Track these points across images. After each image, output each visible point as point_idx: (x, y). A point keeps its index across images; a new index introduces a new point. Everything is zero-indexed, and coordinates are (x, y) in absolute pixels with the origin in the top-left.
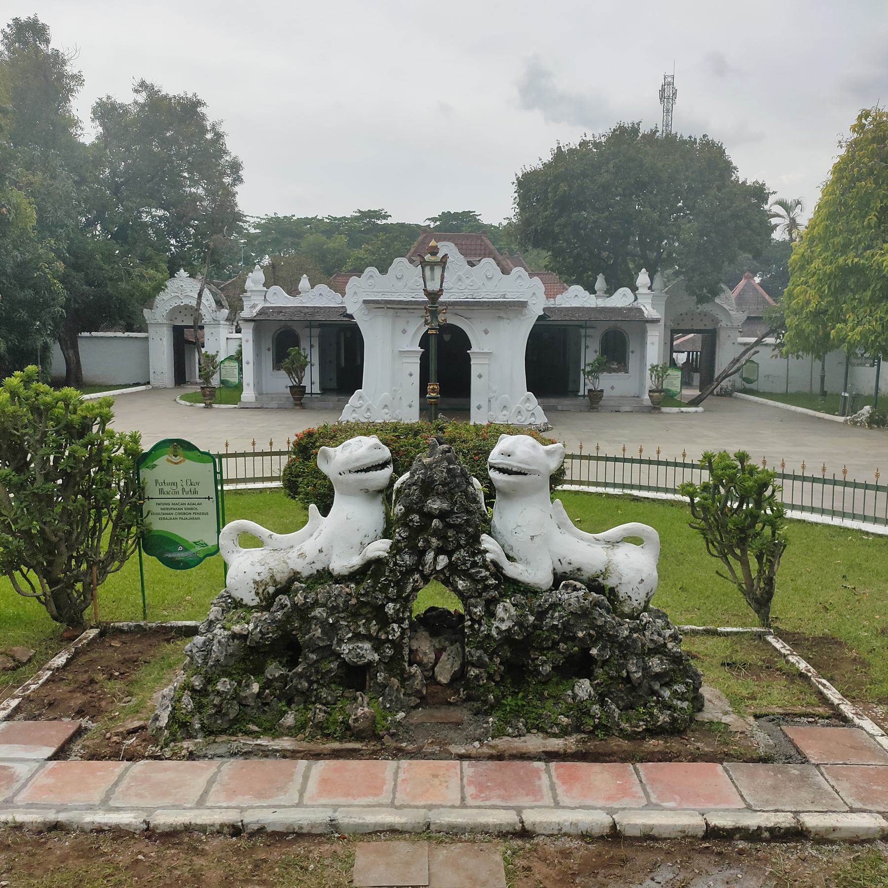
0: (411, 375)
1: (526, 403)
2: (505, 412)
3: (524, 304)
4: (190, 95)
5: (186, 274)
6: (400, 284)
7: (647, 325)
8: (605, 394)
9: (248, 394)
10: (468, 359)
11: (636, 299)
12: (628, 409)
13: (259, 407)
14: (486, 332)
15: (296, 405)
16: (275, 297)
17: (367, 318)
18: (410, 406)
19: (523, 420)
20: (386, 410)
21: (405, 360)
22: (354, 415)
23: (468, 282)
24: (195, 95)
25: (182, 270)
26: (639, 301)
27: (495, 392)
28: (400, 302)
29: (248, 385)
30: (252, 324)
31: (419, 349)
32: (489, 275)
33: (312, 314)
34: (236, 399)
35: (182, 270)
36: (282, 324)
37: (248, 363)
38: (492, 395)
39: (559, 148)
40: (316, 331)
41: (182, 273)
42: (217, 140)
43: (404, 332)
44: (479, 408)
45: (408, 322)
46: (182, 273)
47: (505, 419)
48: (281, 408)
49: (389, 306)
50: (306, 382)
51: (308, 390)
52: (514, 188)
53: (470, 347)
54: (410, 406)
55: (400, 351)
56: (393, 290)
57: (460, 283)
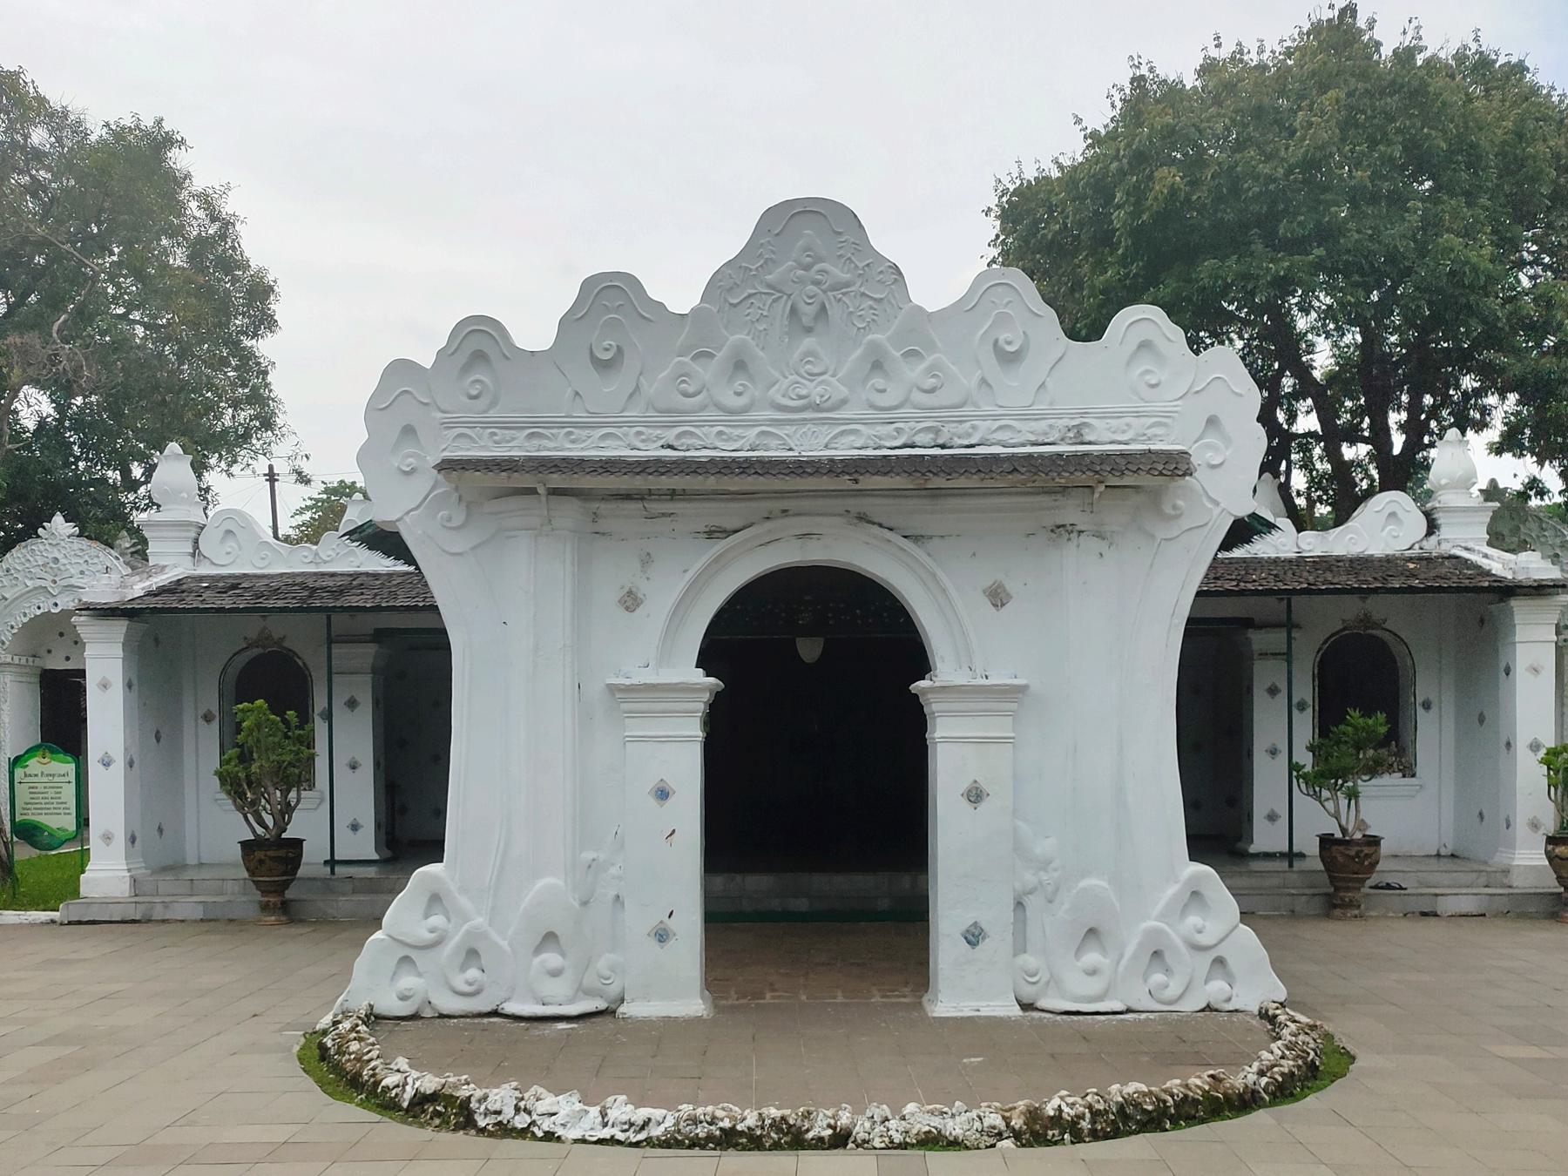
0: (663, 794)
1: (1184, 912)
2: (1092, 958)
3: (1174, 466)
4: (147, 122)
5: (70, 528)
6: (613, 388)
7: (1515, 603)
8: (1385, 848)
9: (107, 873)
10: (911, 729)
11: (1432, 527)
12: (1467, 904)
13: (133, 921)
14: (998, 597)
15: (265, 907)
16: (231, 545)
17: (460, 543)
18: (662, 936)
19: (1174, 989)
20: (552, 959)
21: (636, 728)
22: (408, 982)
23: (914, 372)
24: (159, 122)
25: (58, 518)
26: (1445, 532)
27: (1045, 864)
28: (608, 466)
29: (108, 838)
30: (120, 627)
31: (699, 677)
32: (1011, 339)
33: (341, 592)
34: (60, 886)
35: (58, 518)
36: (252, 627)
37: (107, 763)
38: (1030, 878)
39: (1138, 81)
40: (367, 653)
41: (59, 525)
42: (223, 237)
43: (631, 601)
44: (973, 937)
45: (647, 560)
46: (59, 525)
47: (1094, 986)
48: (215, 922)
49: (557, 480)
50: (306, 825)
51: (314, 854)
52: (992, 226)
53: (920, 664)
54: (662, 936)
55: (613, 689)
56: (580, 415)
57: (878, 381)
